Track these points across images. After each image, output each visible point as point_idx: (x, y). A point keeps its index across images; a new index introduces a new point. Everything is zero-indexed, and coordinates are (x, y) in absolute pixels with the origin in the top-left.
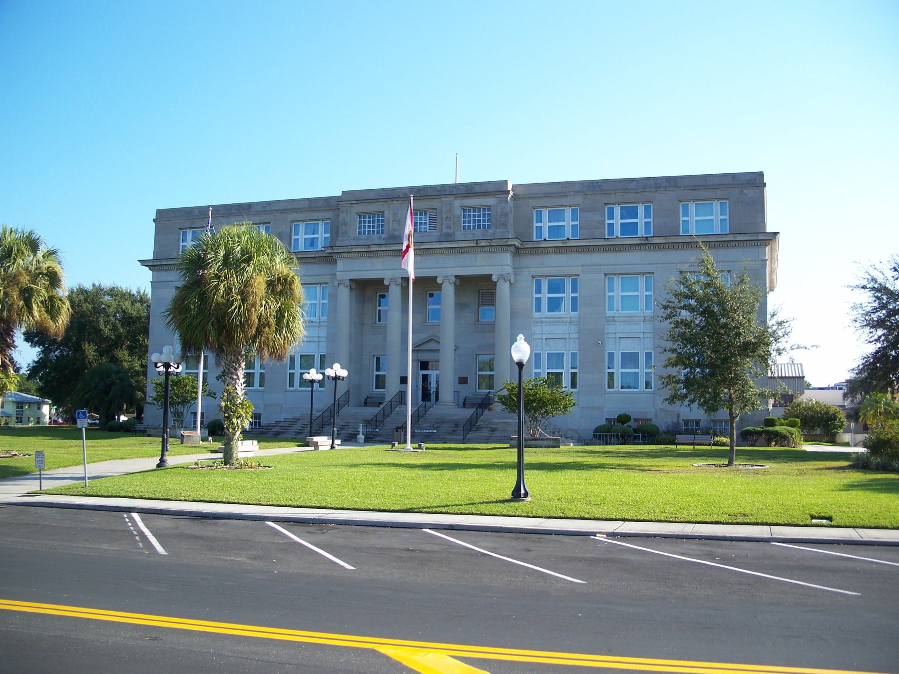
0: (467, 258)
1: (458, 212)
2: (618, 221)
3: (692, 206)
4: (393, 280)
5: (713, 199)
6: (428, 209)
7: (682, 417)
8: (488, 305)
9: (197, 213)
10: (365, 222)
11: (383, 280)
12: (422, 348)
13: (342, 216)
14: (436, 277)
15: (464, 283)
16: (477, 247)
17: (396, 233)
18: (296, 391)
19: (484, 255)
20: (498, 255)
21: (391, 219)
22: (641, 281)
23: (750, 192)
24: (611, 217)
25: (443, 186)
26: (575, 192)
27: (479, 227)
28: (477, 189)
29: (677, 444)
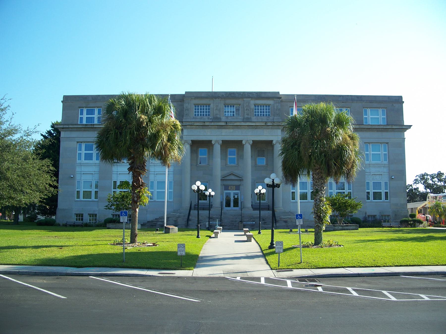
0: (259, 131)
1: (253, 107)
2: (85, 116)
3: (369, 110)
4: (216, 141)
5: (379, 108)
6: (235, 104)
7: (368, 214)
8: (261, 156)
9: (91, 99)
10: (198, 109)
11: (242, 141)
12: (225, 178)
13: (186, 105)
14: (242, 141)
15: (256, 144)
16: (266, 126)
17: (218, 116)
18: (371, 202)
19: (268, 130)
20: (276, 130)
21: (215, 109)
22: (382, 147)
23: (396, 106)
24: (82, 114)
25: (244, 92)
26: (312, 100)
27: (264, 115)
28: (263, 95)
29: (383, 227)
